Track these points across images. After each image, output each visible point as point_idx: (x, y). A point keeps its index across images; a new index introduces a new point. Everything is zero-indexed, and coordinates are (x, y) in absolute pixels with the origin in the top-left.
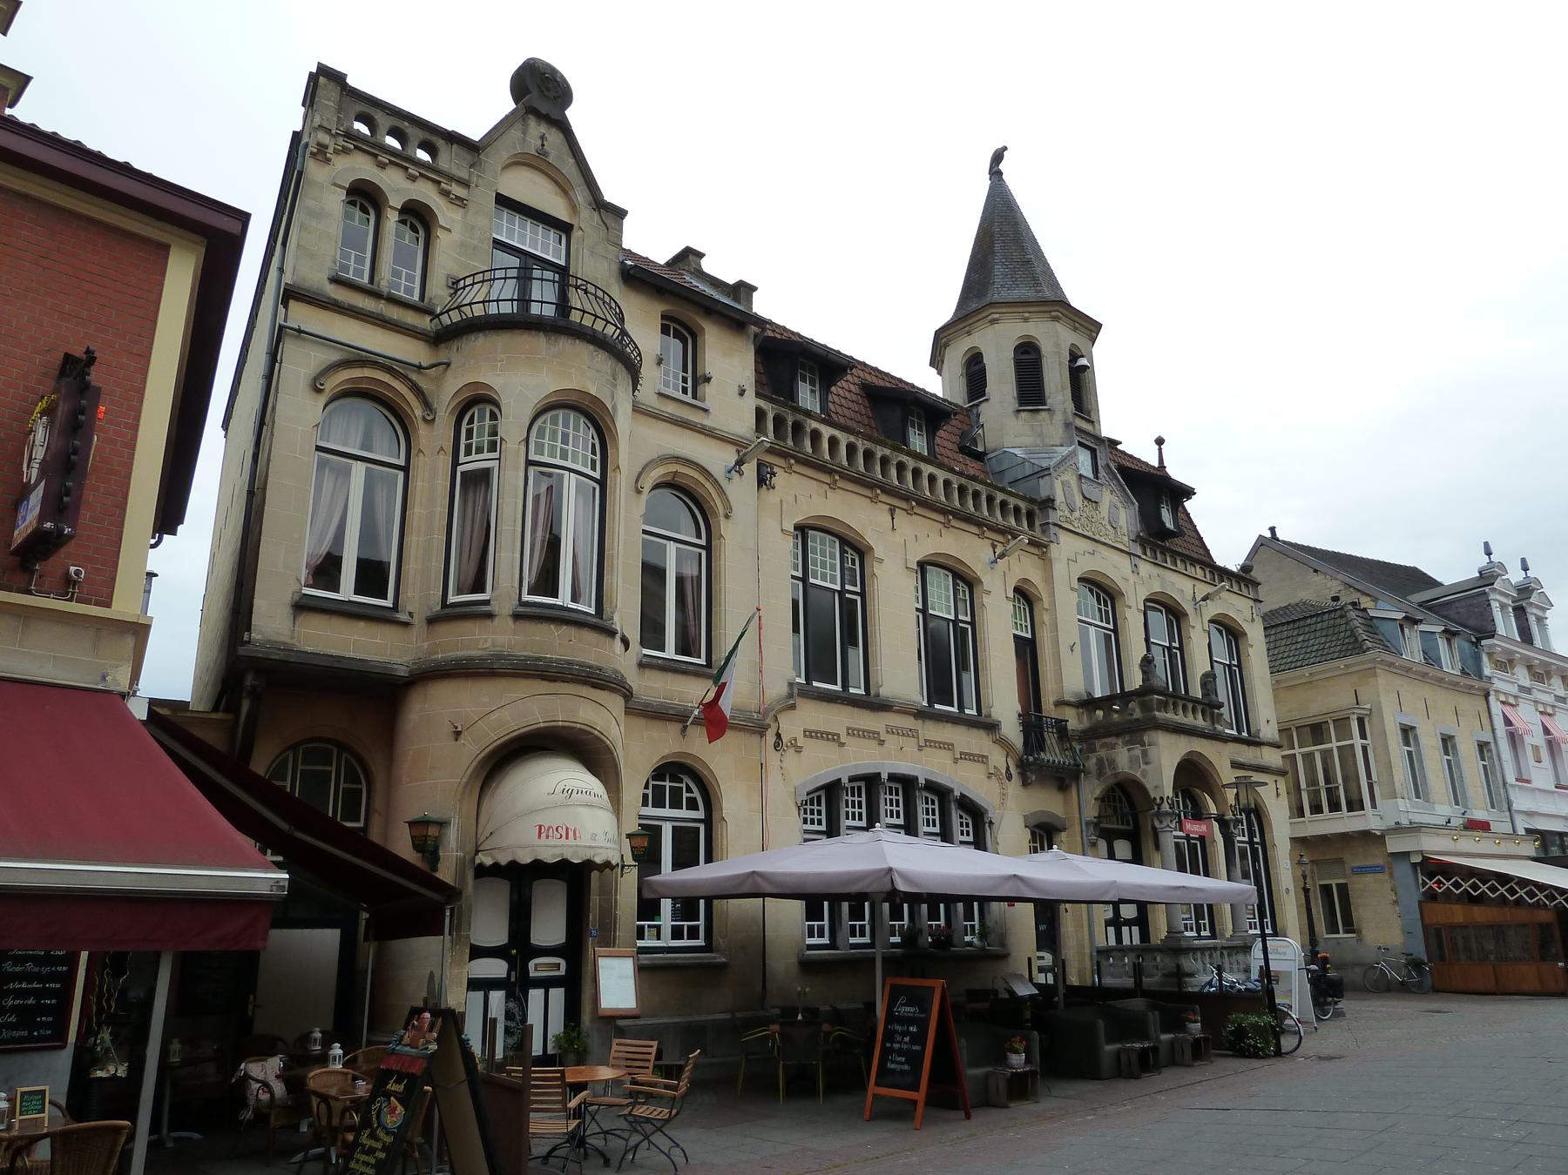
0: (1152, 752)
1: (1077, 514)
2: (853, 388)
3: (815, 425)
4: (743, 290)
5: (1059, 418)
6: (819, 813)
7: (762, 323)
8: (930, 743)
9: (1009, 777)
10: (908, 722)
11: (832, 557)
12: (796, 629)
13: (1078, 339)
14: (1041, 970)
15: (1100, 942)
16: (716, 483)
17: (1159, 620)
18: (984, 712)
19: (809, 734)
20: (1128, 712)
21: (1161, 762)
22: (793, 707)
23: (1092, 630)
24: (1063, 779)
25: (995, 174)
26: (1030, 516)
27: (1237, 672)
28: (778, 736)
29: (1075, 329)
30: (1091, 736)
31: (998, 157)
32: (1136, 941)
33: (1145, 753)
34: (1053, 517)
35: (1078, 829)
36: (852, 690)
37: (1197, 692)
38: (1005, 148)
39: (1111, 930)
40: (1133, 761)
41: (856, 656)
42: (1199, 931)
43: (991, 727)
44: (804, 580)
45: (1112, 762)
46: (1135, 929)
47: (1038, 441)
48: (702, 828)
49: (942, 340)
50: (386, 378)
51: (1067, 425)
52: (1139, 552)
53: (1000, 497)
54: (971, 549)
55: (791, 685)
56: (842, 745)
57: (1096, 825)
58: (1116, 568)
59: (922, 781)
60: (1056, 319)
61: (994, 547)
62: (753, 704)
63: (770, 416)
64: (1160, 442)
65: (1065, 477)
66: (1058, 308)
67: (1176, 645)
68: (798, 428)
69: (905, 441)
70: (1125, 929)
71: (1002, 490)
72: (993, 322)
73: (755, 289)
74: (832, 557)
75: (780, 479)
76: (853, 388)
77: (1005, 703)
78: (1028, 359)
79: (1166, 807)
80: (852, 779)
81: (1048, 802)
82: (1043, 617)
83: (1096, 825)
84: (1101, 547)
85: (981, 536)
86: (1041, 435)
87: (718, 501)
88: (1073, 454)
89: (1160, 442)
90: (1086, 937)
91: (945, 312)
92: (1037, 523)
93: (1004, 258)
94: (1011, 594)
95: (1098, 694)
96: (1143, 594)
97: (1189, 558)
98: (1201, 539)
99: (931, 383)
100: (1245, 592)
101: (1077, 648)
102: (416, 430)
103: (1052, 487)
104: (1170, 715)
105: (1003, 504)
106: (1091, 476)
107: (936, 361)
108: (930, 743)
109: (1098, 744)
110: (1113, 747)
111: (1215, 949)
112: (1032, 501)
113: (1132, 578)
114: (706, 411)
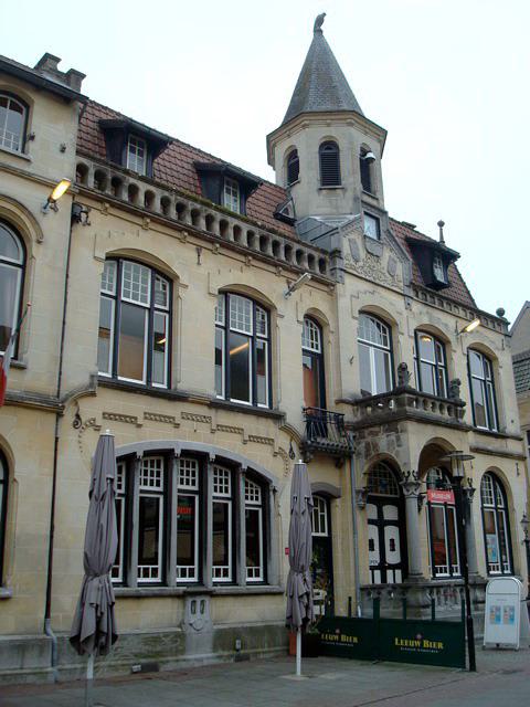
0: (403, 436)
1: (361, 264)
2: (185, 165)
3: (132, 181)
4: (76, 76)
5: (350, 194)
6: (158, 475)
7: (84, 99)
8: (221, 428)
9: (292, 456)
10: (203, 411)
11: (145, 281)
12: (218, 361)
13: (373, 144)
14: (316, 603)
15: (366, 580)
16: (30, 215)
17: (478, 365)
18: (173, 387)
19: (108, 416)
20: (390, 408)
21: (412, 444)
22: (93, 394)
23: (372, 350)
24: (339, 458)
25: (318, 31)
26: (322, 263)
27: (490, 386)
28: (78, 416)
29: (366, 133)
30: (359, 427)
31: (320, 20)
32: (399, 581)
33: (398, 439)
34: (339, 264)
35: (349, 497)
36: (259, 405)
37: (429, 388)
38: (325, 14)
39: (377, 573)
40: (390, 444)
41: (263, 381)
42: (451, 572)
43: (276, 417)
44: (226, 328)
45: (376, 446)
46: (398, 572)
47: (334, 211)
48: (230, 504)
49: (272, 140)
50: (13, 208)
51: (356, 199)
52: (412, 294)
53: (296, 247)
54: (268, 283)
55: (92, 376)
56: (139, 426)
57: (364, 494)
58: (393, 305)
59: (212, 457)
60: (351, 124)
61: (288, 283)
62: (51, 390)
63: (92, 171)
64: (441, 224)
65: (352, 236)
66: (355, 115)
67: (489, 379)
68: (117, 183)
69: (219, 202)
70: (390, 572)
71: (298, 242)
72: (304, 126)
73: (83, 76)
74: (145, 281)
75: (96, 217)
76: (185, 165)
77: (291, 394)
78: (329, 156)
79: (412, 479)
80: (147, 453)
81: (324, 476)
82: (329, 337)
83: (364, 494)
84: (380, 289)
85: (278, 274)
86: (337, 208)
87: (31, 229)
88: (359, 220)
89: (441, 224)
90: (352, 576)
91: (276, 121)
92: (328, 268)
93: (321, 90)
94: (301, 319)
95: (374, 393)
96: (414, 325)
97: (454, 302)
98: (468, 292)
99: (269, 175)
100: (498, 329)
101: (356, 362)
102: (31, 248)
103: (339, 241)
104: (420, 410)
105: (299, 254)
106: (375, 238)
107: (271, 161)
108: (221, 428)
109: (366, 432)
110: (377, 434)
111: (449, 586)
112: (324, 252)
113: (405, 313)
114: (28, 161)
